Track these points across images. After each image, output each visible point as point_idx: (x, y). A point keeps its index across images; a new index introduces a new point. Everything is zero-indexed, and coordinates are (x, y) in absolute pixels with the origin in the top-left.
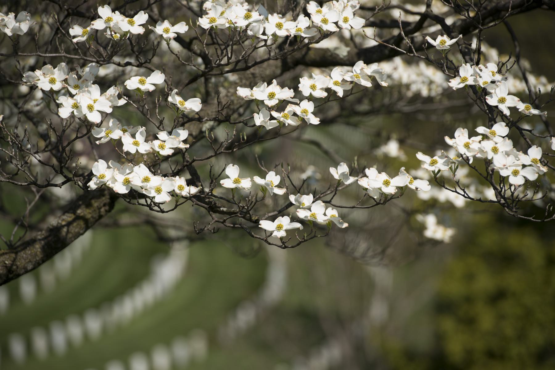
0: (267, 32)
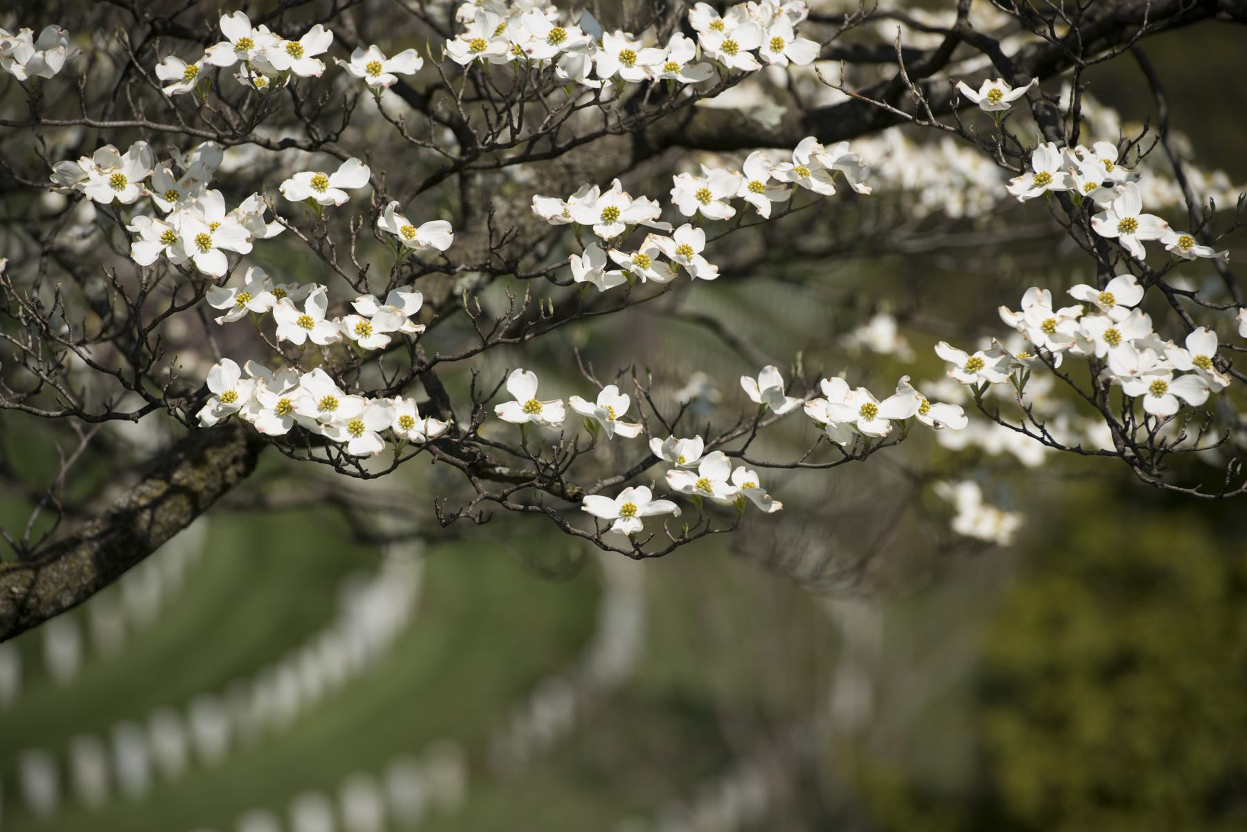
0: (599, 72)
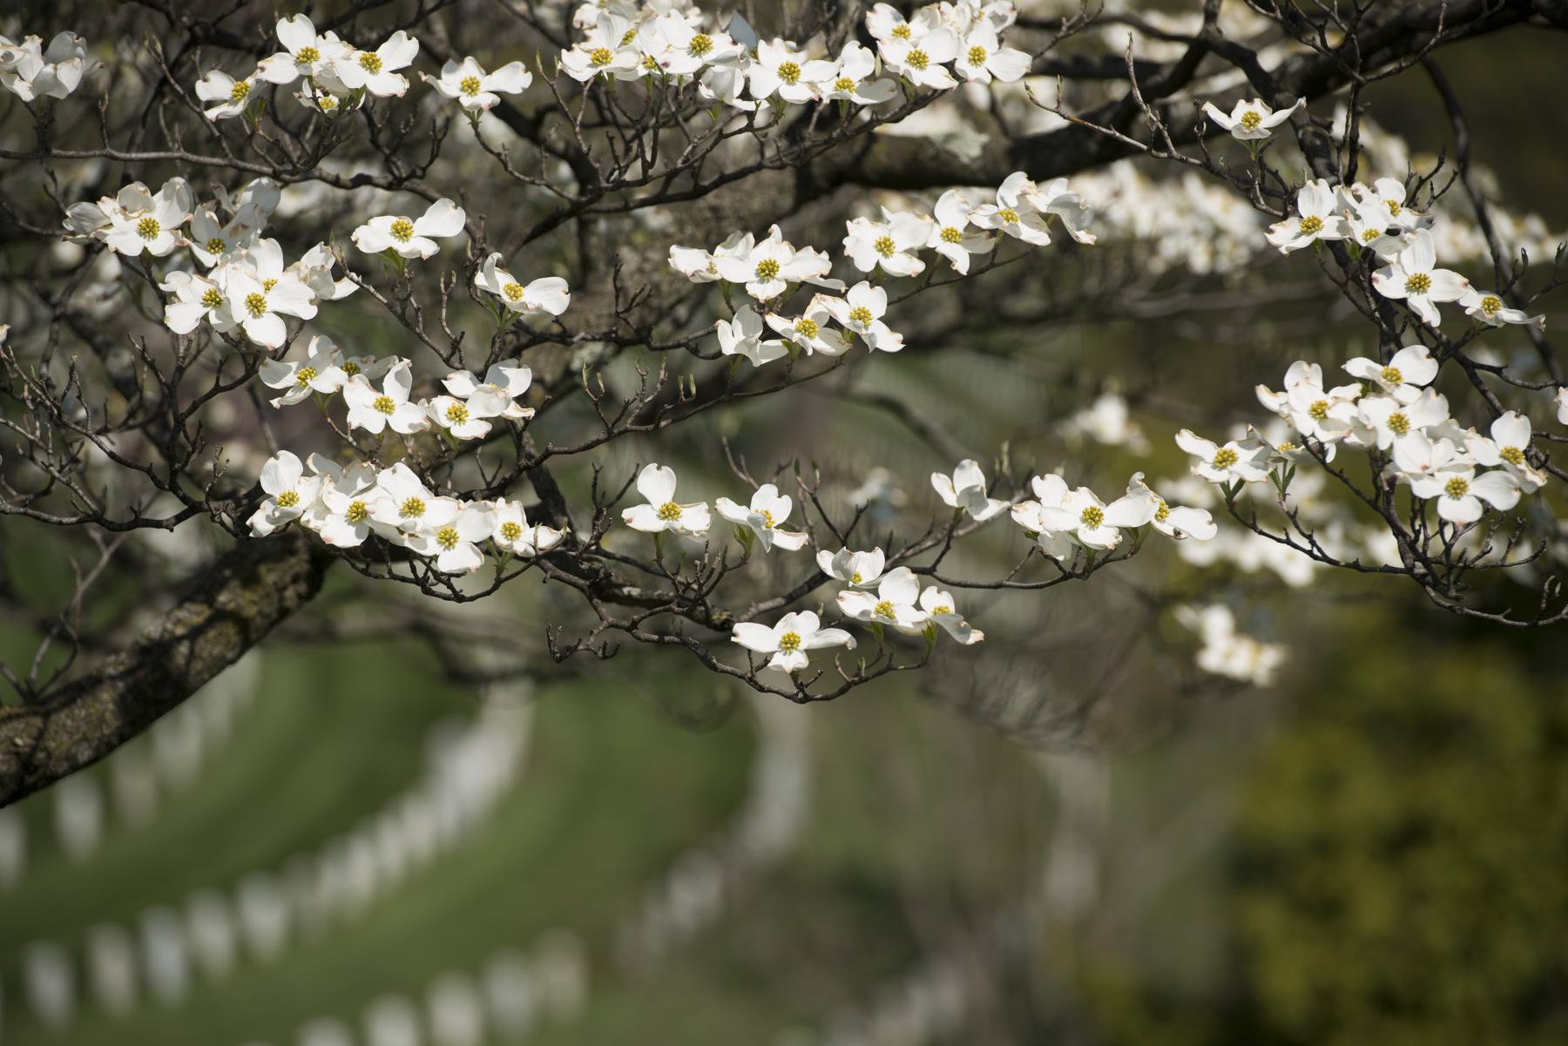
0: (753, 91)
